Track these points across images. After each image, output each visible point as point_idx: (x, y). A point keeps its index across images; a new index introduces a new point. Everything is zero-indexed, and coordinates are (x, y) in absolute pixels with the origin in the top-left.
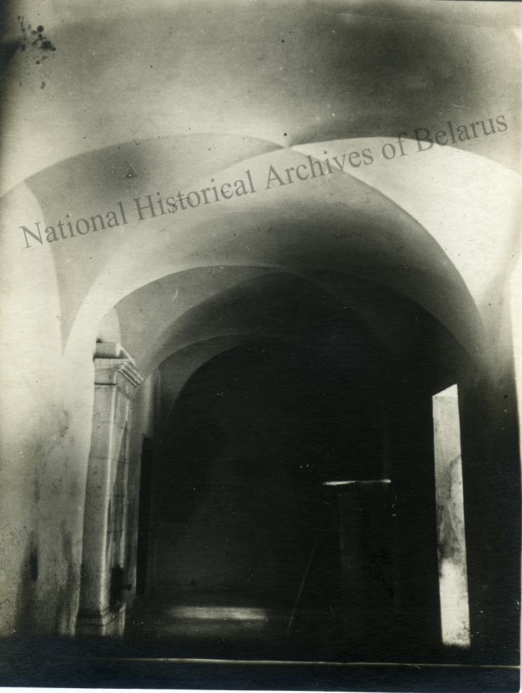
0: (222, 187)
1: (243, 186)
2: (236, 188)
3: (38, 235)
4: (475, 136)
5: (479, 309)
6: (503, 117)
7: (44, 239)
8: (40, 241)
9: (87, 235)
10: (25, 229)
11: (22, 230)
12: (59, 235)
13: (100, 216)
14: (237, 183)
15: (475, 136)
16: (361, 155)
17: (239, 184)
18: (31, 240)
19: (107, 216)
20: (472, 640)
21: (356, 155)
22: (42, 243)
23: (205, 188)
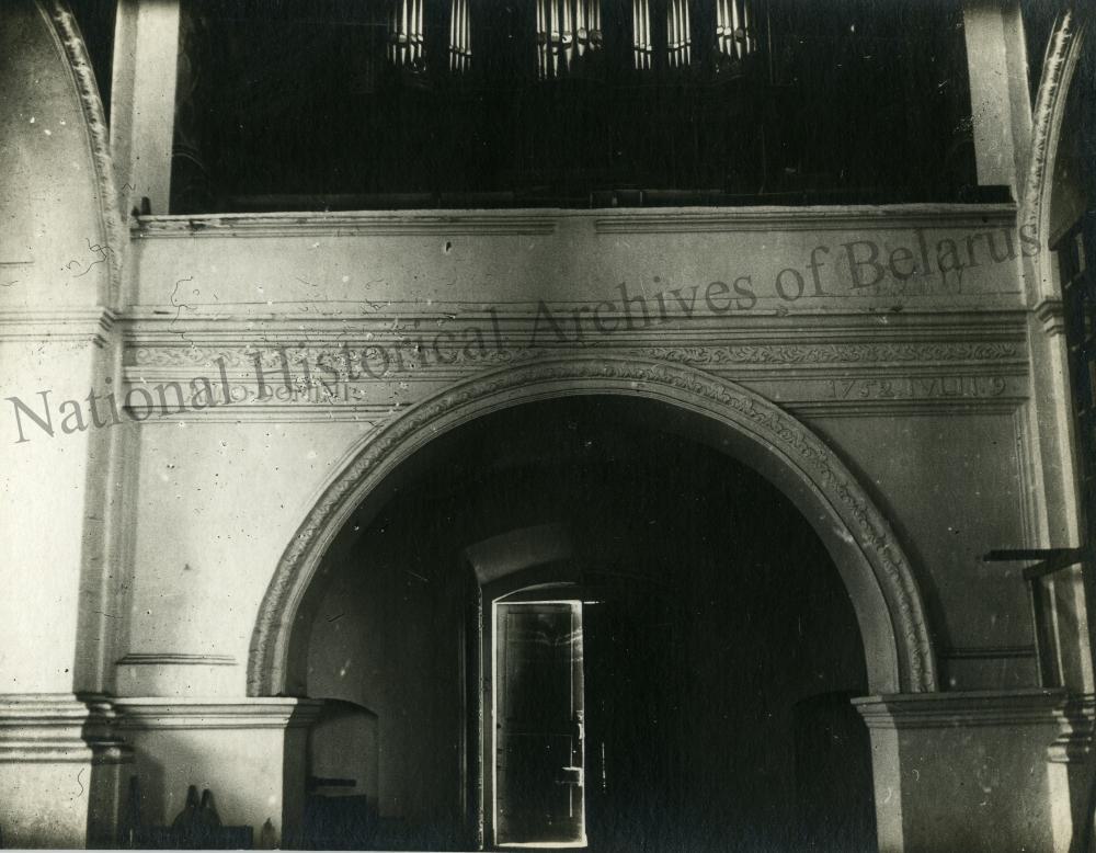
0: (780, 275)
1: (78, 411)
2: (64, 416)
3: (44, 418)
4: (973, 264)
5: (359, 430)
6: (749, 279)
7: (56, 427)
8: (48, 428)
9: (734, 279)
10: (17, 403)
11: (12, 404)
12: (274, 381)
13: (175, 384)
14: (943, 246)
15: (973, 264)
16: (732, 289)
17: (70, 408)
18: (31, 428)
19: (62, 409)
20: (982, 187)
21: (903, 255)
22: (51, 433)
23: (46, 390)
